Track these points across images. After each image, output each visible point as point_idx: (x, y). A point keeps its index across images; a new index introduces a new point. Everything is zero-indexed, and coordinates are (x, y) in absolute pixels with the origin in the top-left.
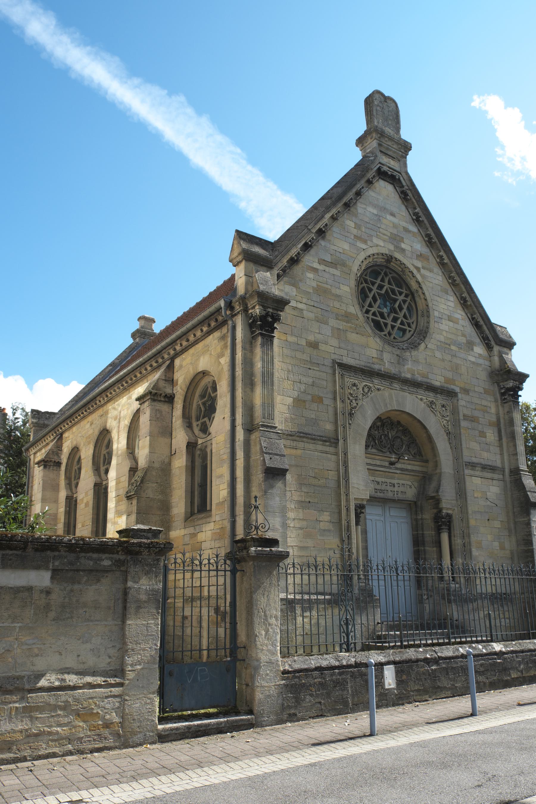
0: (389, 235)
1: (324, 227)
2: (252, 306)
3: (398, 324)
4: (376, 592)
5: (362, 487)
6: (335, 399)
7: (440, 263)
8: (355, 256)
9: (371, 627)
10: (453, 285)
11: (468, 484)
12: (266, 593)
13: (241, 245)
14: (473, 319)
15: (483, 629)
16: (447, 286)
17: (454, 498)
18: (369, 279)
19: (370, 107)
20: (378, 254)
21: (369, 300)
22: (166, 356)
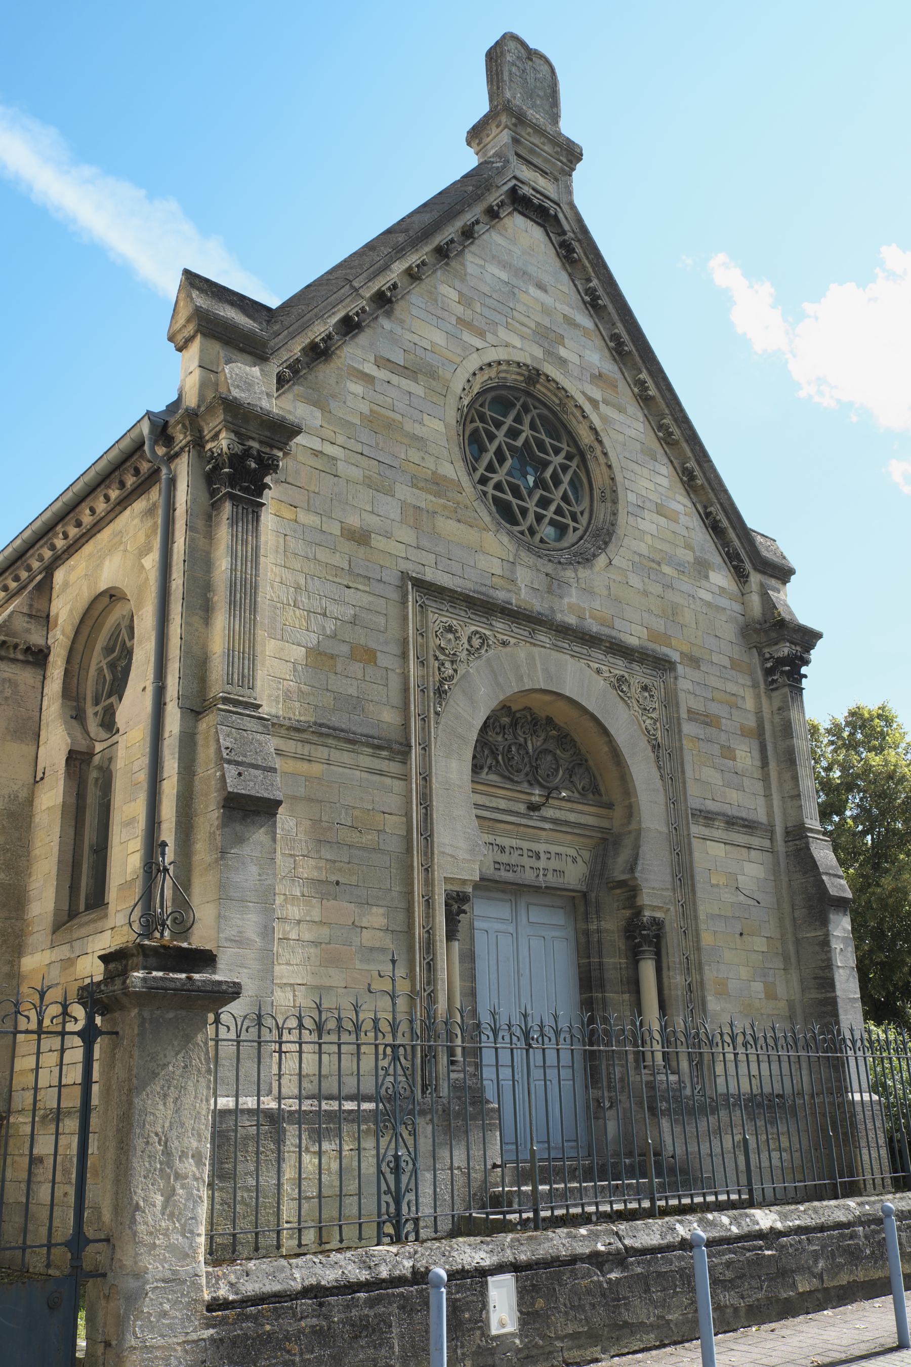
0: (533, 326)
1: (389, 288)
2: (213, 433)
3: (550, 513)
4: (490, 1093)
5: (462, 855)
6: (404, 656)
7: (641, 396)
8: (458, 360)
9: (477, 1176)
10: (668, 443)
11: (697, 855)
12: (173, 1093)
13: (192, 299)
14: (708, 515)
15: (731, 1176)
16: (655, 445)
17: (669, 886)
18: (488, 413)
19: (496, 65)
20: (508, 363)
21: (489, 456)
22: (36, 565)
